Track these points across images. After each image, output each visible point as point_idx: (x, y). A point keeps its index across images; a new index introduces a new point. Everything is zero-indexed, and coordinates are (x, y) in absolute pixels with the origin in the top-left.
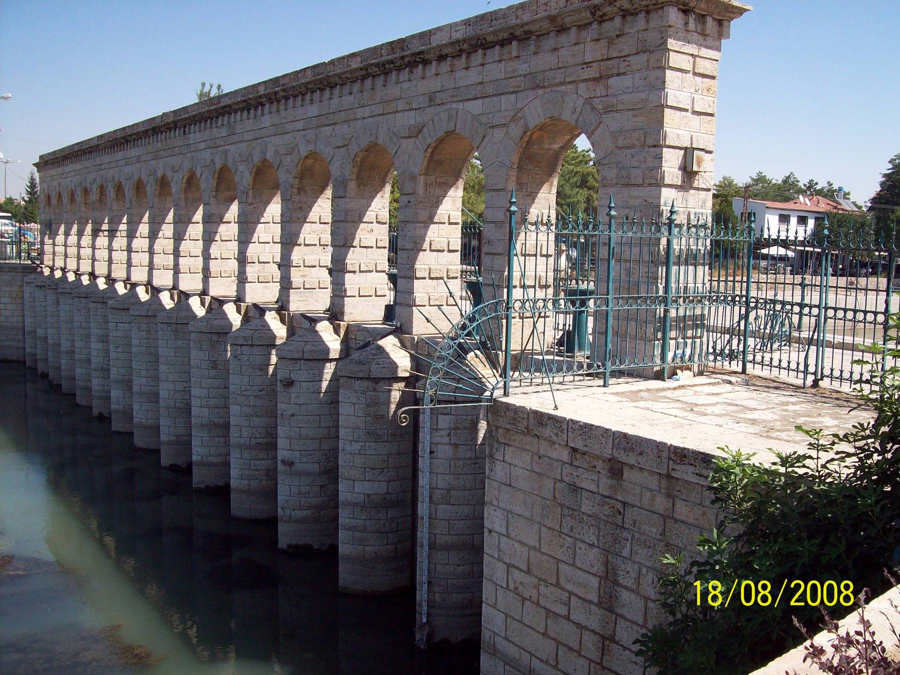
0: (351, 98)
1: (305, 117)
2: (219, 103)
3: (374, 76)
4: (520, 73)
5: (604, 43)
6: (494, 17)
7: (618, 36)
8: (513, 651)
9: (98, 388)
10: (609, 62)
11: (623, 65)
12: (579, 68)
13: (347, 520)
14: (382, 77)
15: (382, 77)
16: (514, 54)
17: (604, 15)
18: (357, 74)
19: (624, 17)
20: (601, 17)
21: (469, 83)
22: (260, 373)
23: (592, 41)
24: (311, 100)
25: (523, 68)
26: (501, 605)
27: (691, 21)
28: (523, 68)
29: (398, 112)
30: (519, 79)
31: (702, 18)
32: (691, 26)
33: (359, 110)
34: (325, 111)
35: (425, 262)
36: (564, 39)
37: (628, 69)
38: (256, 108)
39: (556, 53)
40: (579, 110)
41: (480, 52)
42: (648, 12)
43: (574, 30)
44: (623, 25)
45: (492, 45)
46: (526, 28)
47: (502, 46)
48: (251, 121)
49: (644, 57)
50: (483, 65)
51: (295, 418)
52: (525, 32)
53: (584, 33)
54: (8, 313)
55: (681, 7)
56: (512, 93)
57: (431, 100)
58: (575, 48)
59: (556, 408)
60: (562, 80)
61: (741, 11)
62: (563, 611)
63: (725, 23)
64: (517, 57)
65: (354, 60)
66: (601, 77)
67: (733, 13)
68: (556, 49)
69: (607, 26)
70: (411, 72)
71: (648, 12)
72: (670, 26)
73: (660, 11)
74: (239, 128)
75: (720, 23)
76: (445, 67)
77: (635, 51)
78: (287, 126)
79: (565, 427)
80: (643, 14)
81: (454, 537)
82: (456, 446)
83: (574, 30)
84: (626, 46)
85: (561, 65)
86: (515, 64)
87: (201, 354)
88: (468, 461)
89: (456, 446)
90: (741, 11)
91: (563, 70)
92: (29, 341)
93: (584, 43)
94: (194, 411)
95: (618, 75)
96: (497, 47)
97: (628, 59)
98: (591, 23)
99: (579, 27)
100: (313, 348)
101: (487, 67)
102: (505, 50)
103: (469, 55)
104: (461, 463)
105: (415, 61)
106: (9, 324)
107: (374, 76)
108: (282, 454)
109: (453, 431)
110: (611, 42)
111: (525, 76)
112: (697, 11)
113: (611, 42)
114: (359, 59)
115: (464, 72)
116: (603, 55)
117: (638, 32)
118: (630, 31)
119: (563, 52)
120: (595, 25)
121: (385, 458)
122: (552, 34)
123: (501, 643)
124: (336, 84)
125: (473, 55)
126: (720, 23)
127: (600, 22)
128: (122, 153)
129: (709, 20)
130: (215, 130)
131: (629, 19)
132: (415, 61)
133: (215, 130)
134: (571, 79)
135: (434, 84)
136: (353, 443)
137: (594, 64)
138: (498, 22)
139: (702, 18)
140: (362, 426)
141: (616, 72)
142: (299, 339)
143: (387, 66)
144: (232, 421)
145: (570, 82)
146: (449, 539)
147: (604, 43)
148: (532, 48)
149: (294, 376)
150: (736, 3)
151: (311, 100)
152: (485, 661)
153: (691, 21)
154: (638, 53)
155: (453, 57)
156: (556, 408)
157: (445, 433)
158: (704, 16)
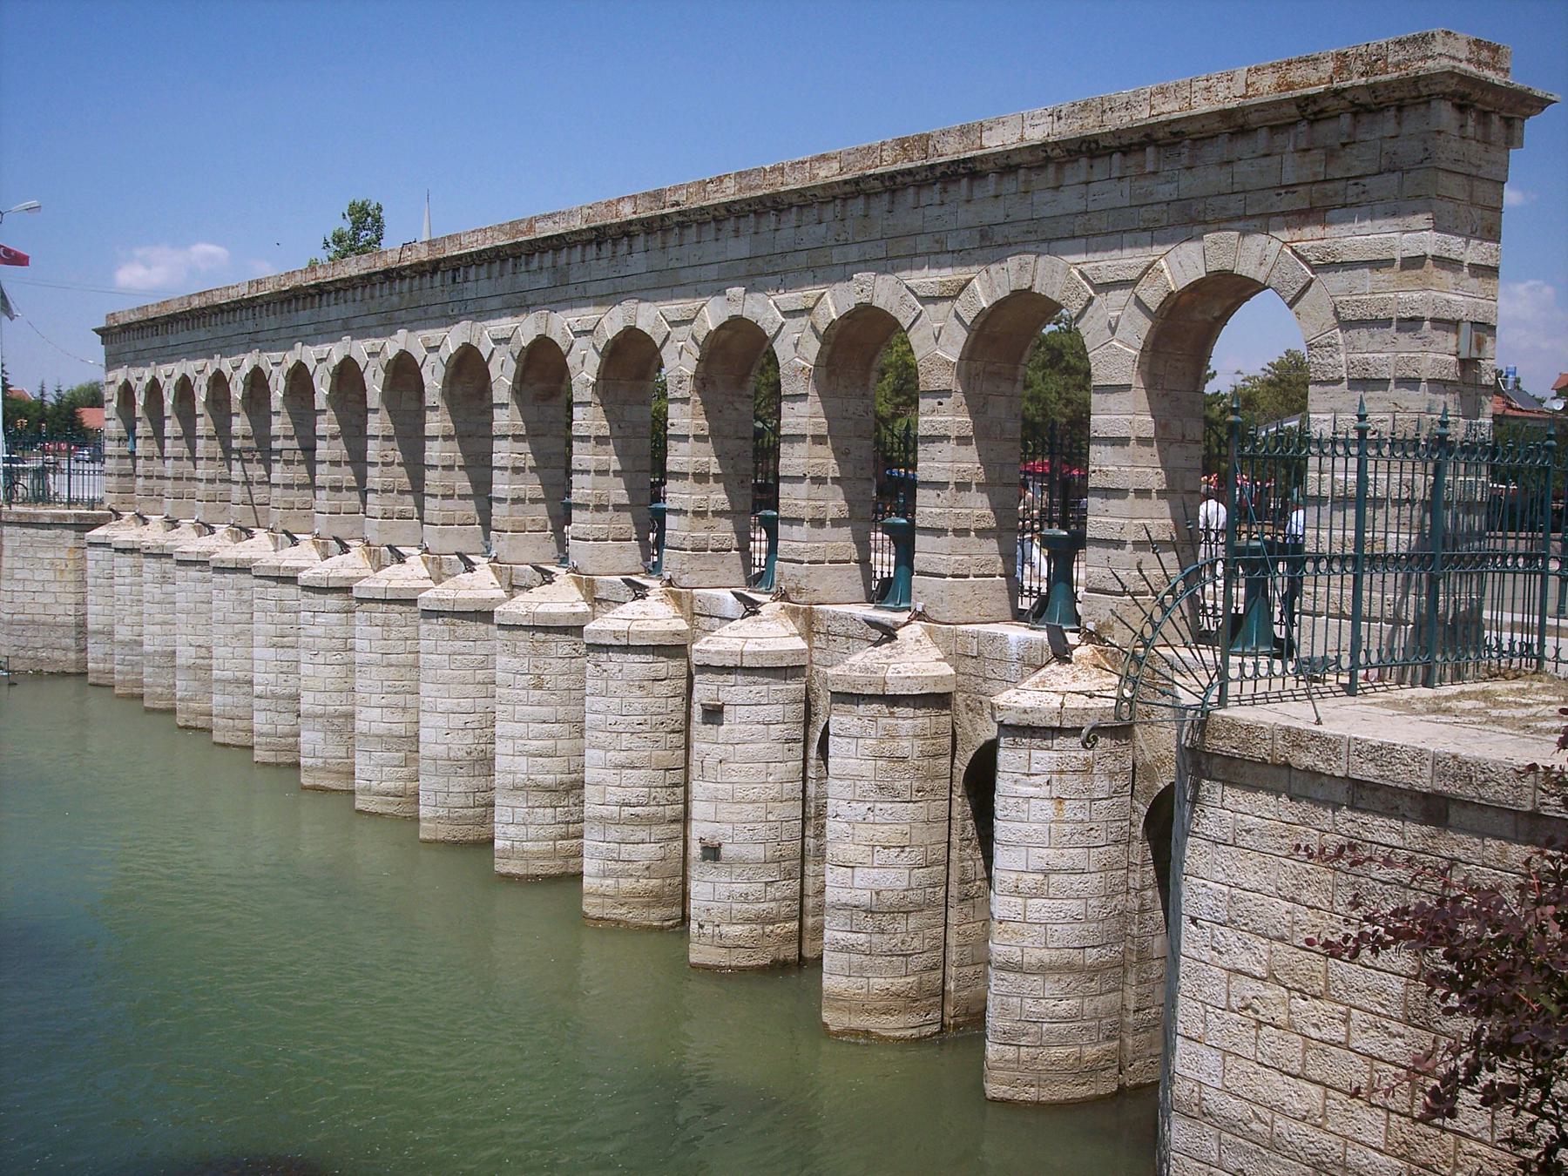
0: (821, 229)
1: (720, 258)
2: (531, 228)
3: (868, 196)
4: (1160, 197)
5: (1317, 155)
6: (1107, 106)
7: (1344, 145)
8: (1235, 1108)
9: (266, 728)
10: (1327, 186)
11: (1352, 190)
12: (1272, 192)
13: (840, 935)
14: (886, 197)
15: (886, 197)
16: (1150, 168)
17: (1321, 111)
18: (837, 191)
19: (1355, 114)
20: (1315, 114)
21: (1060, 211)
22: (639, 693)
23: (1297, 151)
24: (737, 230)
25: (1164, 191)
26: (1213, 1038)
27: (1471, 123)
28: (1164, 191)
29: (916, 255)
30: (1156, 208)
31: (1484, 116)
32: (1470, 130)
33: (835, 251)
34: (764, 250)
35: (677, 494)
36: (1242, 147)
37: (1363, 197)
38: (615, 242)
39: (1227, 169)
40: (1271, 260)
41: (1084, 162)
42: (1400, 109)
43: (1263, 133)
44: (1355, 127)
45: (1108, 152)
46: (1176, 128)
47: (1124, 154)
48: (604, 263)
49: (1394, 178)
50: (1088, 183)
51: (725, 766)
52: (1174, 134)
53: (1280, 139)
54: (49, 599)
55: (1457, 101)
56: (1145, 230)
57: (983, 237)
58: (1265, 162)
59: (1319, 722)
60: (1241, 212)
61: (1543, 103)
62: (1339, 1033)
63: (1517, 123)
64: (1154, 173)
65: (824, 165)
66: (1311, 210)
67: (1532, 107)
68: (1229, 162)
69: (1322, 128)
70: (945, 190)
71: (1400, 109)
72: (1439, 132)
73: (1423, 108)
74: (576, 274)
75: (1508, 123)
76: (1010, 185)
77: (1375, 169)
78: (683, 273)
79: (1343, 748)
80: (1393, 112)
81: (1054, 952)
82: (1060, 800)
83: (1263, 133)
84: (1356, 161)
85: (1237, 188)
86: (1146, 183)
87: (516, 663)
88: (1079, 827)
89: (1060, 800)
90: (1543, 103)
91: (1240, 196)
92: (95, 650)
93: (1281, 154)
94: (501, 763)
95: (1344, 206)
96: (1117, 157)
97: (1362, 181)
98: (1295, 124)
99: (1271, 128)
100: (758, 649)
101: (1094, 187)
102: (1132, 160)
103: (1060, 166)
104: (1067, 828)
105: (955, 173)
106: (50, 619)
107: (868, 196)
108: (697, 830)
109: (1055, 776)
110: (1331, 154)
111: (1168, 203)
112: (1479, 106)
113: (1331, 154)
114: (836, 166)
115: (1048, 195)
116: (1315, 174)
117: (1383, 138)
118: (1367, 137)
119: (1241, 168)
120: (1303, 127)
121: (906, 828)
122: (1223, 139)
123: (1214, 1100)
124: (791, 205)
125: (1068, 166)
126: (1508, 123)
127: (1311, 123)
128: (308, 312)
129: (1495, 118)
130: (523, 277)
131: (1365, 118)
132: (955, 173)
133: (523, 277)
134: (1257, 211)
135: (993, 213)
136: (854, 804)
137: (1300, 188)
138: (1116, 114)
139: (1484, 116)
140: (870, 774)
141: (1341, 201)
142: (732, 634)
143: (899, 179)
144: (590, 775)
145: (1252, 217)
146: (1045, 955)
147: (1317, 155)
148: (1185, 161)
149: (724, 697)
150: (1539, 93)
151: (737, 230)
152: (1178, 1133)
153: (1471, 123)
154: (1380, 173)
155: (1029, 169)
156: (1319, 722)
157: (1041, 780)
158: (1486, 114)
